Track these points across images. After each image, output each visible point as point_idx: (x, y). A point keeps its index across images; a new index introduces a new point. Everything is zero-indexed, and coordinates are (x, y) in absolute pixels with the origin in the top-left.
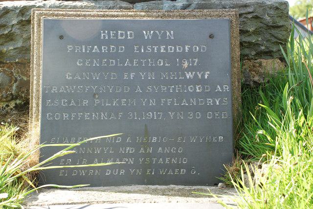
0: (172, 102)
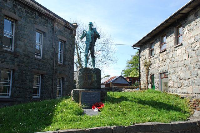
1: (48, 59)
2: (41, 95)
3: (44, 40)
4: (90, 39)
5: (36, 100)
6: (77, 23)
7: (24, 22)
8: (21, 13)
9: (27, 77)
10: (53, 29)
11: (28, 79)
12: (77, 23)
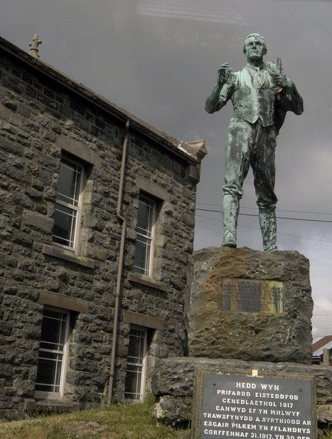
0: (277, 429)
7: (20, 124)
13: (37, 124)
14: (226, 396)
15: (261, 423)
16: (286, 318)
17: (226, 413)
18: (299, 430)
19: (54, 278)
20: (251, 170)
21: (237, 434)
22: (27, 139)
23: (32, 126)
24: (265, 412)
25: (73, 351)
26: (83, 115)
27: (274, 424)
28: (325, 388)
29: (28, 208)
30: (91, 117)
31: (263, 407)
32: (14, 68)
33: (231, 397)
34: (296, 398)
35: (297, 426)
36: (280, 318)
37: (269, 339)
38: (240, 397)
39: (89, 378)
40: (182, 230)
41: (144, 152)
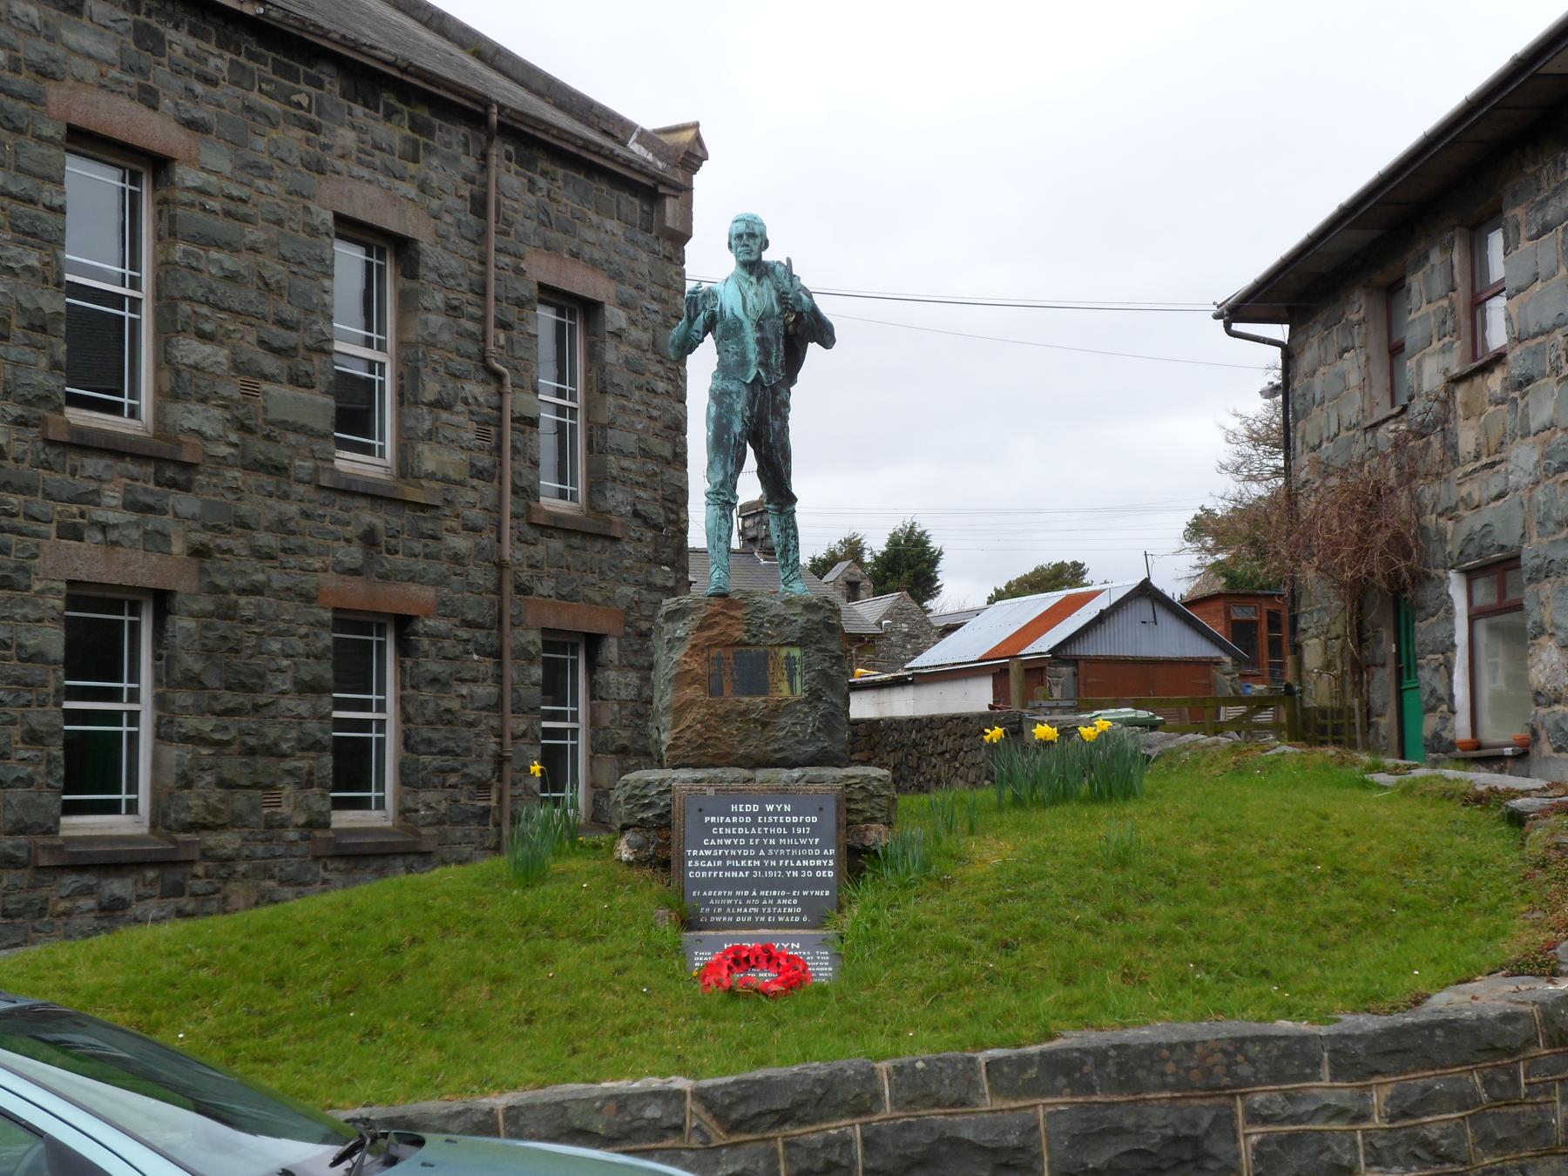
1: (445, 479)
2: (400, 800)
3: (407, 302)
4: (753, 355)
5: (365, 857)
6: (696, 125)
7: (225, 166)
8: (199, 88)
9: (275, 646)
10: (479, 206)
11: (286, 663)
12: (696, 125)
13: (266, 160)
14: (718, 825)
15: (767, 857)
16: (806, 701)
17: (718, 847)
18: (819, 863)
19: (348, 541)
20: (750, 451)
21: (734, 874)
22: (244, 201)
23: (255, 166)
24: (772, 842)
25: (411, 710)
26: (377, 111)
27: (785, 857)
28: (862, 800)
29: (266, 378)
30: (398, 112)
31: (770, 836)
32: (193, 19)
33: (725, 825)
34: (815, 819)
35: (815, 858)
36: (799, 702)
37: (781, 734)
38: (738, 825)
39: (454, 770)
40: (656, 374)
41: (542, 182)
